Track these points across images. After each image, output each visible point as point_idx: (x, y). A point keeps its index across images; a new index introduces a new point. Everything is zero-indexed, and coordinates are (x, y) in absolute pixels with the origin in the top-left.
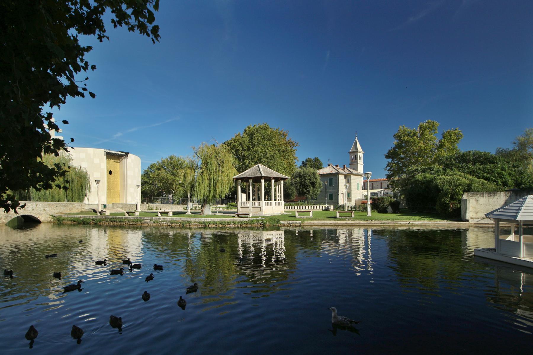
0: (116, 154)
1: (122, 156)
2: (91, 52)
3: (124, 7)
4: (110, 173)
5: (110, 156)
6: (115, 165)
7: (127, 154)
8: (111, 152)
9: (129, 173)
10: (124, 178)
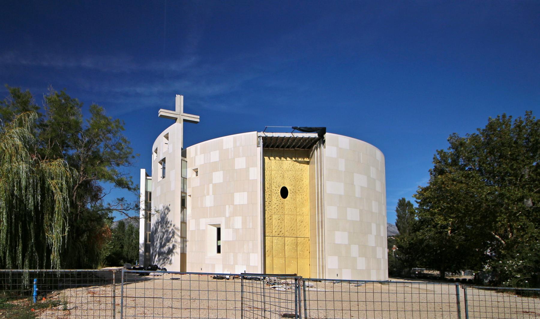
5: (272, 148)
6: (284, 168)
7: (322, 132)
8: (276, 135)
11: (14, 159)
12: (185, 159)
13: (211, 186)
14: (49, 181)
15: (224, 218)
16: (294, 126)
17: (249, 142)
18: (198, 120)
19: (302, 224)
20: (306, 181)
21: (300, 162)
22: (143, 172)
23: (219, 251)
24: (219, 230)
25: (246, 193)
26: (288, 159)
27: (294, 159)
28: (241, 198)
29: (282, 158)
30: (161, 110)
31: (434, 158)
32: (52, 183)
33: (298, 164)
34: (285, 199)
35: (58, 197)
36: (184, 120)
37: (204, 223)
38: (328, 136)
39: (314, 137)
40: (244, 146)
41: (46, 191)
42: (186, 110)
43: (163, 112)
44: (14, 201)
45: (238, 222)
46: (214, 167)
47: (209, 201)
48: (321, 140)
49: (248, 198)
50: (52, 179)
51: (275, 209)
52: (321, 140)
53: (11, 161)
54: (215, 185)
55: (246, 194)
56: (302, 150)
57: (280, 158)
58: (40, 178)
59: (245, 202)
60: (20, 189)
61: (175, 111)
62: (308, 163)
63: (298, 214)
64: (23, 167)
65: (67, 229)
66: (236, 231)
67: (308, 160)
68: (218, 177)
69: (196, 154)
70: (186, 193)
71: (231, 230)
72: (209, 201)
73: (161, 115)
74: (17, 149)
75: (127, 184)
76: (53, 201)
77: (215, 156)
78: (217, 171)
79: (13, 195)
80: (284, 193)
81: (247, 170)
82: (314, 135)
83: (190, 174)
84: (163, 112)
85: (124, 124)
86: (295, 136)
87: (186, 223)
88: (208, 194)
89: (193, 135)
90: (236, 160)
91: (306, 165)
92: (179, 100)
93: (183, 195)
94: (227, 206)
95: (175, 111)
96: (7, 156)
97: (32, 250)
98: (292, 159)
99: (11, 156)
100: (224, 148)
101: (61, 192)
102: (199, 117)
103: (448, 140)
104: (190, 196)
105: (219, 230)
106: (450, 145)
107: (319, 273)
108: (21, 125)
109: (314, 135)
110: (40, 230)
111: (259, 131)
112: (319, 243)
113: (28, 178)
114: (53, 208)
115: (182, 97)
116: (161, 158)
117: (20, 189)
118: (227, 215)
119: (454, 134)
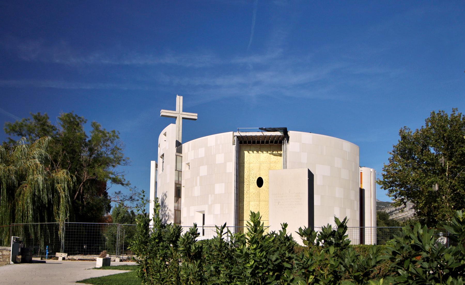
11: (35, 172)
12: (181, 155)
13: (198, 178)
14: (56, 185)
16: (261, 127)
18: (196, 118)
21: (275, 155)
22: (153, 163)
24: (204, 215)
25: (224, 184)
26: (255, 152)
30: (162, 110)
32: (58, 186)
35: (62, 194)
36: (183, 118)
38: (290, 133)
40: (222, 144)
41: (54, 191)
42: (185, 109)
43: (164, 112)
44: (36, 199)
45: (217, 208)
50: (58, 183)
52: (286, 136)
53: (33, 175)
56: (275, 144)
57: (258, 152)
58: (51, 183)
60: (39, 191)
61: (175, 110)
62: (280, 155)
64: (40, 178)
65: (68, 215)
68: (203, 171)
70: (181, 185)
72: (197, 191)
73: (162, 116)
74: (37, 167)
75: (120, 181)
76: (59, 197)
77: (202, 152)
79: (34, 195)
80: (260, 182)
82: (278, 134)
83: (184, 168)
84: (164, 112)
85: (119, 133)
87: (180, 211)
88: (196, 186)
89: (191, 131)
91: (279, 157)
92: (179, 100)
93: (178, 186)
94: (210, 195)
95: (175, 110)
96: (31, 171)
97: (46, 228)
99: (33, 171)
101: (64, 191)
102: (197, 115)
105: (204, 215)
108: (39, 147)
109: (278, 134)
110: (51, 217)
111: (234, 131)
113: (43, 184)
114: (59, 202)
115: (182, 97)
116: (162, 154)
117: (39, 191)
118: (210, 203)
119: (404, 127)
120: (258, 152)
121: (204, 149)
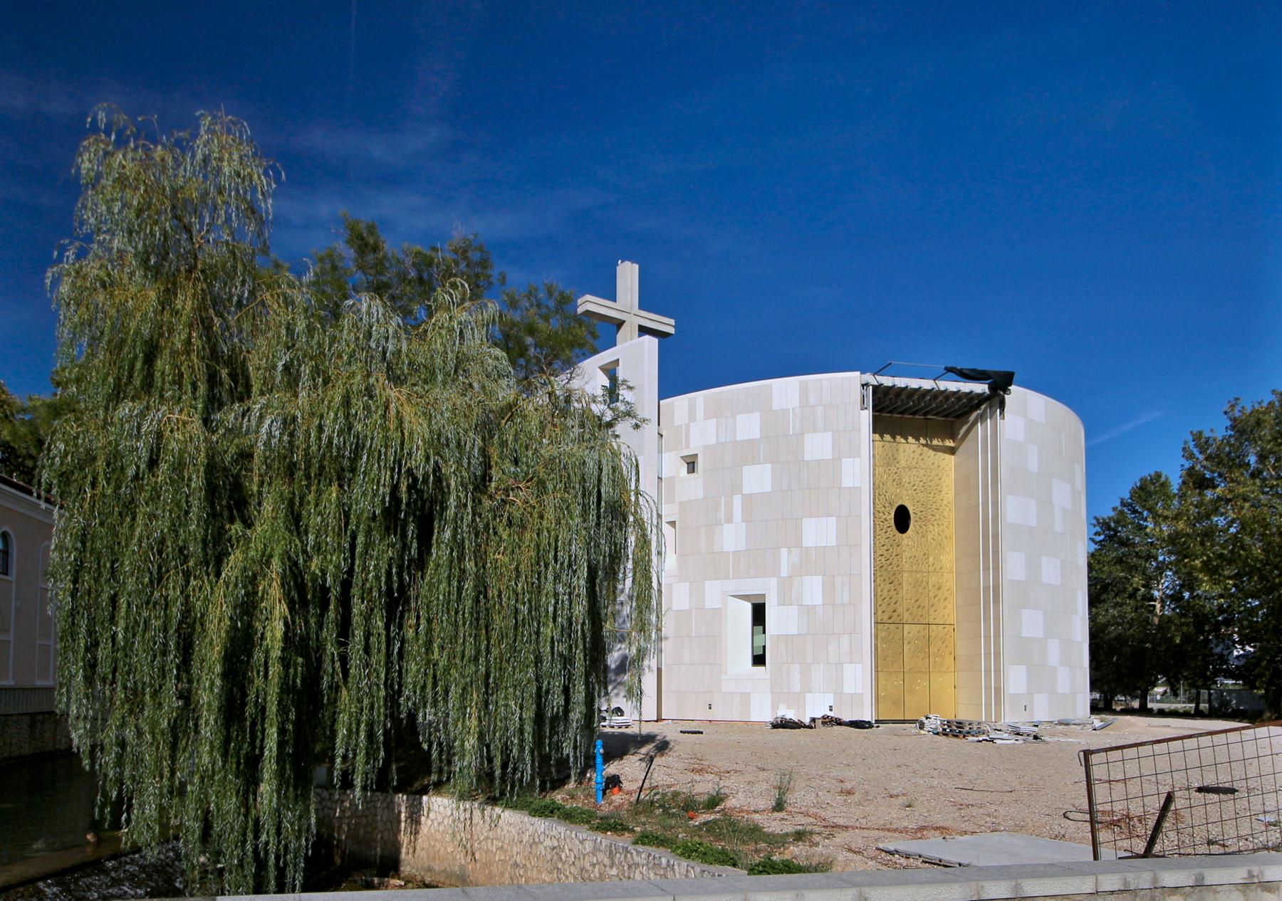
0: (935, 394)
1: (973, 402)
2: (1275, 388)
3: (87, 768)
4: (902, 519)
5: (895, 413)
6: (929, 467)
7: (1001, 383)
8: (901, 382)
9: (1016, 510)
10: (983, 541)
13: (737, 500)
15: (774, 581)
17: (842, 393)
18: (672, 331)
19: (940, 593)
20: (949, 492)
21: (935, 449)
23: (759, 660)
25: (833, 521)
26: (911, 439)
27: (922, 441)
28: (818, 532)
29: (898, 438)
31: (1184, 449)
33: (931, 453)
34: (904, 536)
37: (714, 593)
38: (1015, 394)
39: (967, 391)
43: (590, 303)
45: (812, 590)
46: (748, 453)
47: (732, 537)
48: (996, 400)
49: (840, 531)
51: (883, 559)
52: (996, 399)
54: (749, 499)
55: (832, 521)
59: (832, 542)
61: (615, 301)
62: (952, 451)
63: (931, 569)
66: (808, 610)
67: (952, 444)
69: (692, 417)
71: (794, 610)
72: (732, 537)
77: (749, 427)
78: (755, 461)
81: (836, 463)
82: (981, 388)
86: (942, 388)
88: (729, 519)
90: (808, 437)
91: (947, 456)
92: (628, 275)
94: (784, 551)
95: (615, 301)
98: (918, 439)
100: (775, 407)
102: (672, 322)
103: (1226, 413)
104: (673, 524)
106: (1229, 423)
107: (988, 706)
109: (981, 388)
112: (987, 637)
115: (636, 267)
118: (784, 573)
120: (894, 438)
121: (756, 416)
